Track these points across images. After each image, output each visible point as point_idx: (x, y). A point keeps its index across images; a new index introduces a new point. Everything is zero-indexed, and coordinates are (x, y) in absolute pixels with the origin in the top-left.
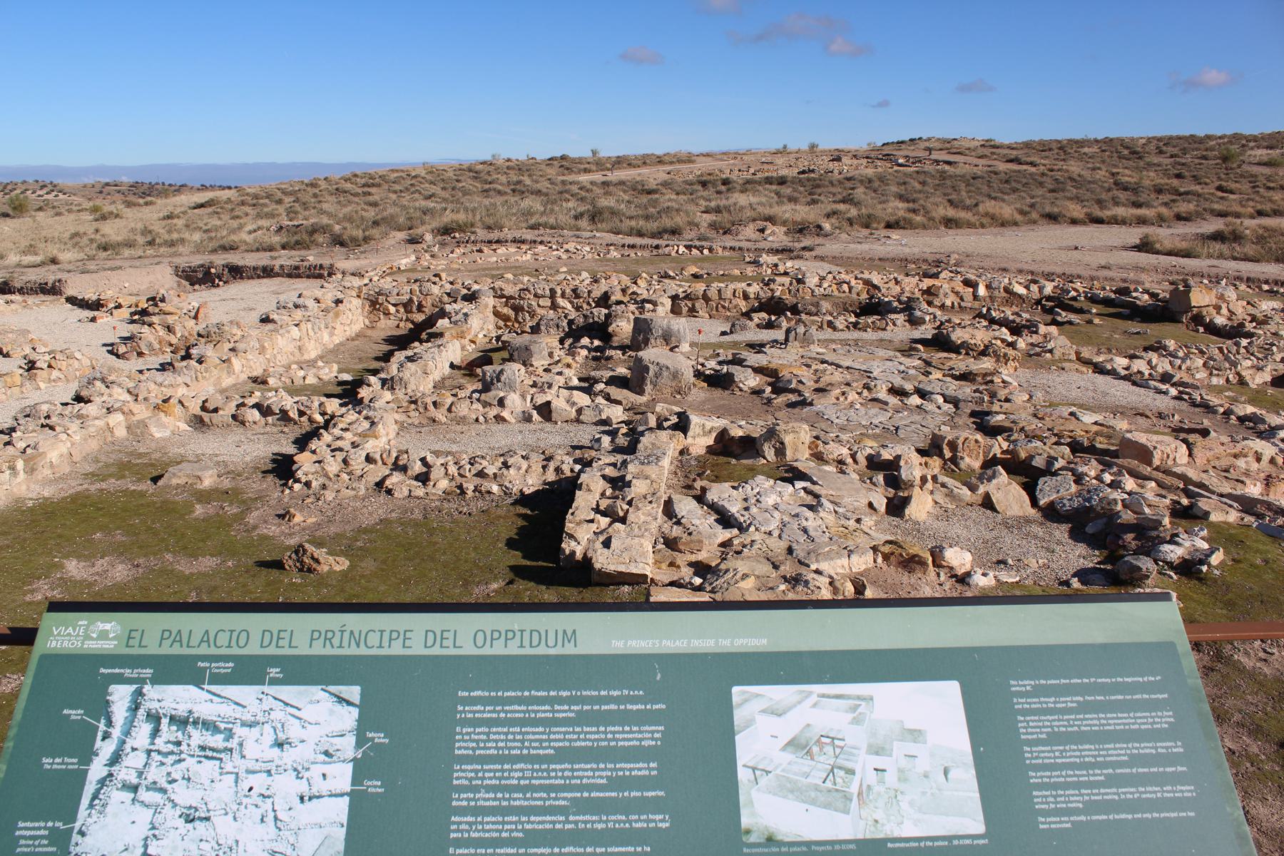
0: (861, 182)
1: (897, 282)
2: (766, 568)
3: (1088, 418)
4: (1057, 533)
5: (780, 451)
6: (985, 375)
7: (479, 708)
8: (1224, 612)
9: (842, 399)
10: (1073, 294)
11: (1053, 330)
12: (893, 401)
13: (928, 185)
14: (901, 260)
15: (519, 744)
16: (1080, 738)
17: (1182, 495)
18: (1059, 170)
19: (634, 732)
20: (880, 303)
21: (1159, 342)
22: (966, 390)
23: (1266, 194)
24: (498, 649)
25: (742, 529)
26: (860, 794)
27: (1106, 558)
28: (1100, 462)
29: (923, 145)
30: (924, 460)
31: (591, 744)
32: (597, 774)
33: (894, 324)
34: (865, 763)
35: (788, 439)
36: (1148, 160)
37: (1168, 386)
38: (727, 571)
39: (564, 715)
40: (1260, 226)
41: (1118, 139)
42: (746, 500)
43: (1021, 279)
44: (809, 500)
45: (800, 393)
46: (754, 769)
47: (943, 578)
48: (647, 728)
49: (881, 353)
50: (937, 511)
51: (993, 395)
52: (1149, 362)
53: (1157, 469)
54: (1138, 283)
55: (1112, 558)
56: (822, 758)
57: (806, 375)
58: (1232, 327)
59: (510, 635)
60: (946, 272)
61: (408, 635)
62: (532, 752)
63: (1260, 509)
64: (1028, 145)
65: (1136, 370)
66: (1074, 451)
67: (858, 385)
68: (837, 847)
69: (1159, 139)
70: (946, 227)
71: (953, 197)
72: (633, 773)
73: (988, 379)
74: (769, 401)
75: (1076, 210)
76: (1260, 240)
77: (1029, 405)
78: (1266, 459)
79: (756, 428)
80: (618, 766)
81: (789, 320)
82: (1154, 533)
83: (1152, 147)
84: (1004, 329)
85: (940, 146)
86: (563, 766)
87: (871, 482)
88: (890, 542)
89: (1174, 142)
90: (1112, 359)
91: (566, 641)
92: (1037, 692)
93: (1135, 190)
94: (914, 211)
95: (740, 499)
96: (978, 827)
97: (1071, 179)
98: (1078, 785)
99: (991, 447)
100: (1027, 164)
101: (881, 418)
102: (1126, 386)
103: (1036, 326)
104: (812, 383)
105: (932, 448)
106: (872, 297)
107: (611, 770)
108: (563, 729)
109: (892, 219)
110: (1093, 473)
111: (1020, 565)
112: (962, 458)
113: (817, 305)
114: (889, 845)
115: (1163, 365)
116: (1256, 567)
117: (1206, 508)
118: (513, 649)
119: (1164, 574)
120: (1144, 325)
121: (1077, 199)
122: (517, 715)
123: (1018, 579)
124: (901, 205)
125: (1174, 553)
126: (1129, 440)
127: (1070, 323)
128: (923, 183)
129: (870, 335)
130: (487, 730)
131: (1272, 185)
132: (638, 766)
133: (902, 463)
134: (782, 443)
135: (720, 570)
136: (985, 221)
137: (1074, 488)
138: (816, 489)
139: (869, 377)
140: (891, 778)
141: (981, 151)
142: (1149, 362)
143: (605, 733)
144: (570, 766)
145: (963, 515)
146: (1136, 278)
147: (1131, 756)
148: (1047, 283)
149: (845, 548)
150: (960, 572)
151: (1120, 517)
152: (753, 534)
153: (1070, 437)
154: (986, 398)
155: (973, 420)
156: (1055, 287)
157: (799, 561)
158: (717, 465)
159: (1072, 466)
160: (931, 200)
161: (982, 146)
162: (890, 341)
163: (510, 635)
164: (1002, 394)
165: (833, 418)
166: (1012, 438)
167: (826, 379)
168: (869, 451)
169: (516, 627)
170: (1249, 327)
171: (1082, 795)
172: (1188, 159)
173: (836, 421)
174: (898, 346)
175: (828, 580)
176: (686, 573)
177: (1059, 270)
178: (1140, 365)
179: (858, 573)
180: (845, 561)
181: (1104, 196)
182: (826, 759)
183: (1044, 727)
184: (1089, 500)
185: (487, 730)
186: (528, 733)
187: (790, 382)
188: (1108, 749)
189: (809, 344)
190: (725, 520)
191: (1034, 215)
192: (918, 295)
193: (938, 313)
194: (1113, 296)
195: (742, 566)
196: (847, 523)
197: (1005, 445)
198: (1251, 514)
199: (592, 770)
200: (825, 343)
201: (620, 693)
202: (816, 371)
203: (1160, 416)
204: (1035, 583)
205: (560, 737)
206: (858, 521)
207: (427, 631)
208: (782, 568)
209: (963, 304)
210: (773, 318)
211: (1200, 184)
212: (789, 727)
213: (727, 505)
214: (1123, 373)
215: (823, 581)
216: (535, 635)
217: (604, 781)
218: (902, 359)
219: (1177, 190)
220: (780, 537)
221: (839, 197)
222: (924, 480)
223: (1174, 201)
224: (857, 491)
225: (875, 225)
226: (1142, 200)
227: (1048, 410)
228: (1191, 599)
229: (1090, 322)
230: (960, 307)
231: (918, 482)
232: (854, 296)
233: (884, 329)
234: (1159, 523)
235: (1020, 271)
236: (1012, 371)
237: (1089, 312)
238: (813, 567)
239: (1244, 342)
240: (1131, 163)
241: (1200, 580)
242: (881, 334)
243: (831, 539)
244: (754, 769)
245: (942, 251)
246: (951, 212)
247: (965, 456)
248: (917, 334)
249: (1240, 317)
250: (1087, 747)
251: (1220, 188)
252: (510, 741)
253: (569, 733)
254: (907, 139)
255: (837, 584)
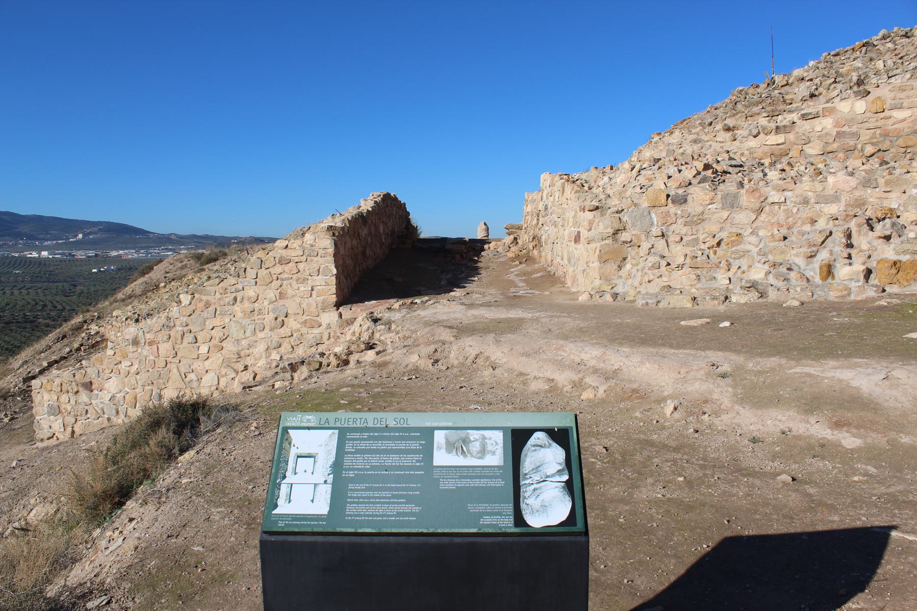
174: (170, 261)
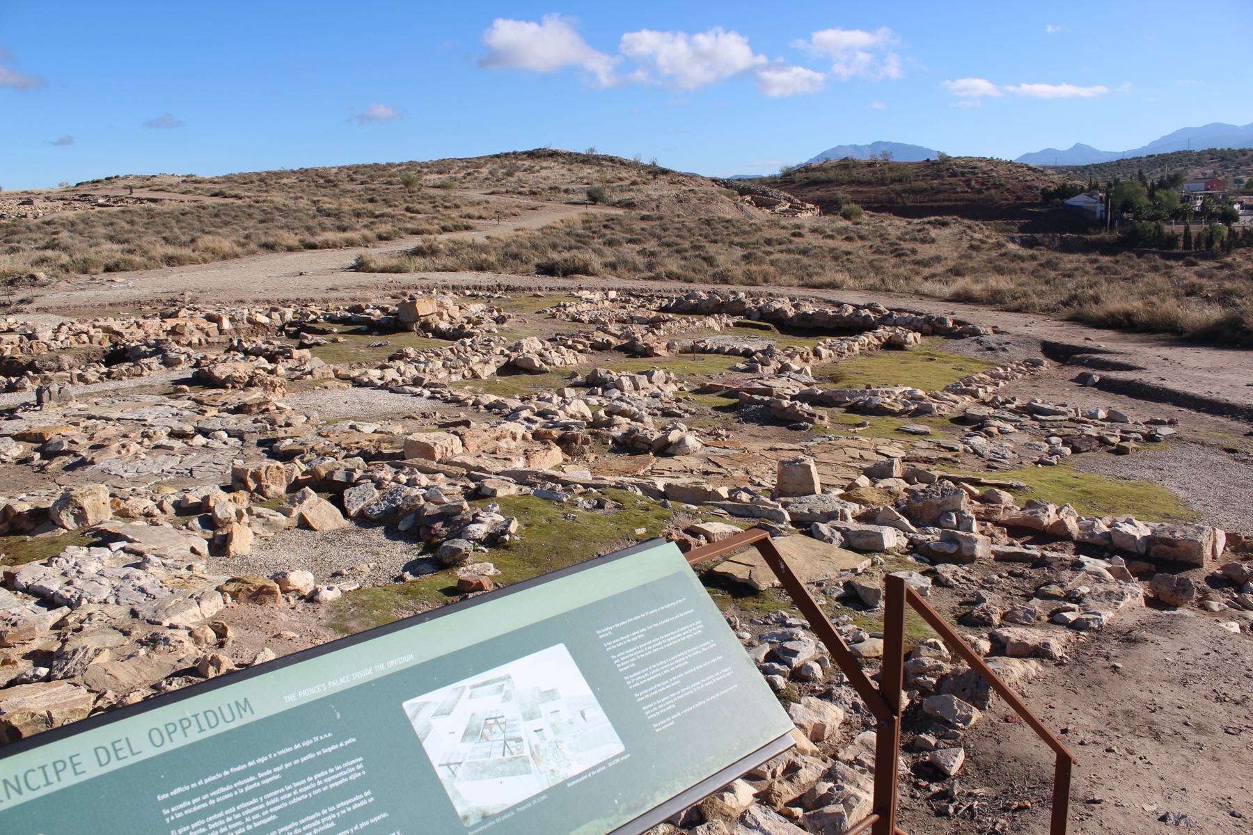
0: (63, 225)
1: (139, 326)
2: (117, 638)
3: (368, 428)
4: (374, 536)
5: (81, 516)
6: (260, 404)
7: (185, 804)
8: (533, 569)
9: (124, 452)
10: (312, 317)
11: (306, 352)
12: (178, 444)
13: (137, 224)
14: (134, 303)
15: (240, 823)
16: (656, 658)
17: (468, 481)
18: (264, 201)
19: (339, 771)
20: (125, 350)
21: (401, 351)
22: (245, 423)
23: (445, 213)
24: (179, 741)
25: (73, 605)
26: (532, 754)
27: (424, 548)
28: (392, 466)
29: (122, 183)
30: (232, 495)
31: (306, 796)
32: (323, 820)
33: (150, 369)
34: (525, 729)
35: (87, 503)
36: (342, 187)
37: (420, 389)
38: (75, 652)
39: (270, 779)
40: (449, 240)
41: (312, 169)
42: (65, 574)
43: (259, 308)
44: (132, 559)
45: (75, 454)
46: (448, 765)
47: (293, 602)
48: (348, 764)
49: (147, 399)
50: (258, 542)
51: (273, 422)
52: (398, 370)
53: (440, 462)
54: (365, 300)
55: (430, 547)
56: (494, 737)
57: (75, 433)
58: (454, 330)
59: (186, 723)
60: (185, 310)
61: (75, 760)
62: (256, 825)
63: (531, 479)
64: (229, 179)
65: (390, 379)
66: (366, 460)
67: (136, 435)
68: (534, 802)
69: (349, 168)
70: (169, 265)
71: (167, 234)
72: (354, 807)
73: (264, 407)
74: (42, 468)
75: (291, 239)
76: (452, 252)
77: (308, 426)
78: (519, 437)
79: (44, 497)
80: (338, 806)
81: (33, 380)
82: (458, 518)
83: (343, 175)
84: (261, 359)
85: (140, 184)
86: (290, 826)
87: (187, 528)
88: (233, 580)
89: (362, 170)
90: (366, 372)
91: (242, 712)
92: (617, 633)
93: (337, 215)
94: (130, 252)
95: (57, 574)
96: (619, 747)
97: (276, 208)
98: (666, 693)
99: (292, 471)
100: (232, 197)
101: (172, 463)
102: (385, 393)
103: (290, 352)
104: (86, 441)
105: (236, 483)
106: (116, 344)
107: (334, 812)
108: (276, 793)
109: (111, 262)
110: (389, 477)
111: (354, 573)
112: (267, 487)
113: (57, 359)
114: (569, 785)
115: (411, 371)
116: (545, 526)
117: (492, 487)
118: (194, 736)
119: (478, 550)
120: (383, 337)
121: (288, 227)
122: (226, 797)
123: (358, 586)
124: (115, 247)
125: (479, 530)
126: (412, 442)
127: (318, 344)
128: (132, 223)
129: (126, 383)
130: (203, 822)
131: (448, 204)
132: (355, 799)
133: (212, 504)
134: (81, 508)
135: (67, 653)
136: (206, 255)
137: (377, 493)
138: (135, 546)
139: (145, 425)
140: (548, 732)
141: (184, 187)
142: (398, 370)
143: (314, 781)
144: (296, 824)
145: (283, 540)
146: (362, 296)
147: (689, 659)
148: (286, 309)
149: (191, 597)
150: (307, 592)
151: (426, 510)
152: (86, 608)
153: (358, 448)
154: (269, 427)
155: (262, 449)
156: (294, 313)
157: (148, 621)
158: (10, 545)
159: (369, 474)
160: (145, 239)
161: (184, 181)
162: (151, 386)
163: (186, 723)
164: (281, 420)
165: (121, 472)
166: (306, 459)
167: (99, 437)
168: (174, 498)
169: (188, 715)
170: (468, 328)
171: (672, 698)
172: (375, 185)
173: (125, 475)
175: (186, 632)
176: (26, 667)
177: (293, 296)
178: (391, 374)
179: (212, 618)
180: (196, 609)
181: (311, 223)
182: (497, 737)
183: (631, 658)
184: (394, 501)
185: (203, 822)
186: (244, 809)
187: (61, 444)
188: (674, 660)
189: (67, 402)
190: (48, 600)
191: (253, 246)
192: (163, 336)
193: (191, 351)
194: (349, 315)
195: (89, 642)
196: (179, 573)
197: (304, 468)
198: (526, 485)
199: (317, 818)
200: (82, 397)
201: (311, 742)
202: (86, 428)
203: (424, 415)
204: (373, 585)
205: (276, 801)
206: (190, 568)
207: (95, 750)
208: (134, 633)
209: (210, 340)
210: (13, 380)
211: (390, 206)
212: (459, 721)
213: (45, 585)
214: (380, 383)
215: (182, 634)
216: (210, 715)
217: (333, 824)
218: (172, 402)
219: (373, 213)
220: (117, 602)
221: (42, 243)
222: (239, 515)
223: (372, 223)
224: (177, 539)
225: (93, 270)
226: (345, 224)
227: (330, 427)
228: (506, 565)
229: (335, 341)
230: (207, 342)
231: (234, 517)
232: (96, 345)
233: (140, 375)
234: (461, 507)
235: (257, 301)
236: (280, 396)
237: (331, 332)
238: (166, 623)
239: (468, 341)
240: (328, 191)
241: (506, 547)
242: (138, 381)
243: (172, 592)
244: (448, 765)
245: (173, 289)
246: (171, 250)
247: (269, 484)
248: (176, 374)
249: (459, 321)
250: (661, 663)
251: (408, 209)
252: (231, 823)
253: (282, 794)
254: (103, 178)
255: (198, 633)
